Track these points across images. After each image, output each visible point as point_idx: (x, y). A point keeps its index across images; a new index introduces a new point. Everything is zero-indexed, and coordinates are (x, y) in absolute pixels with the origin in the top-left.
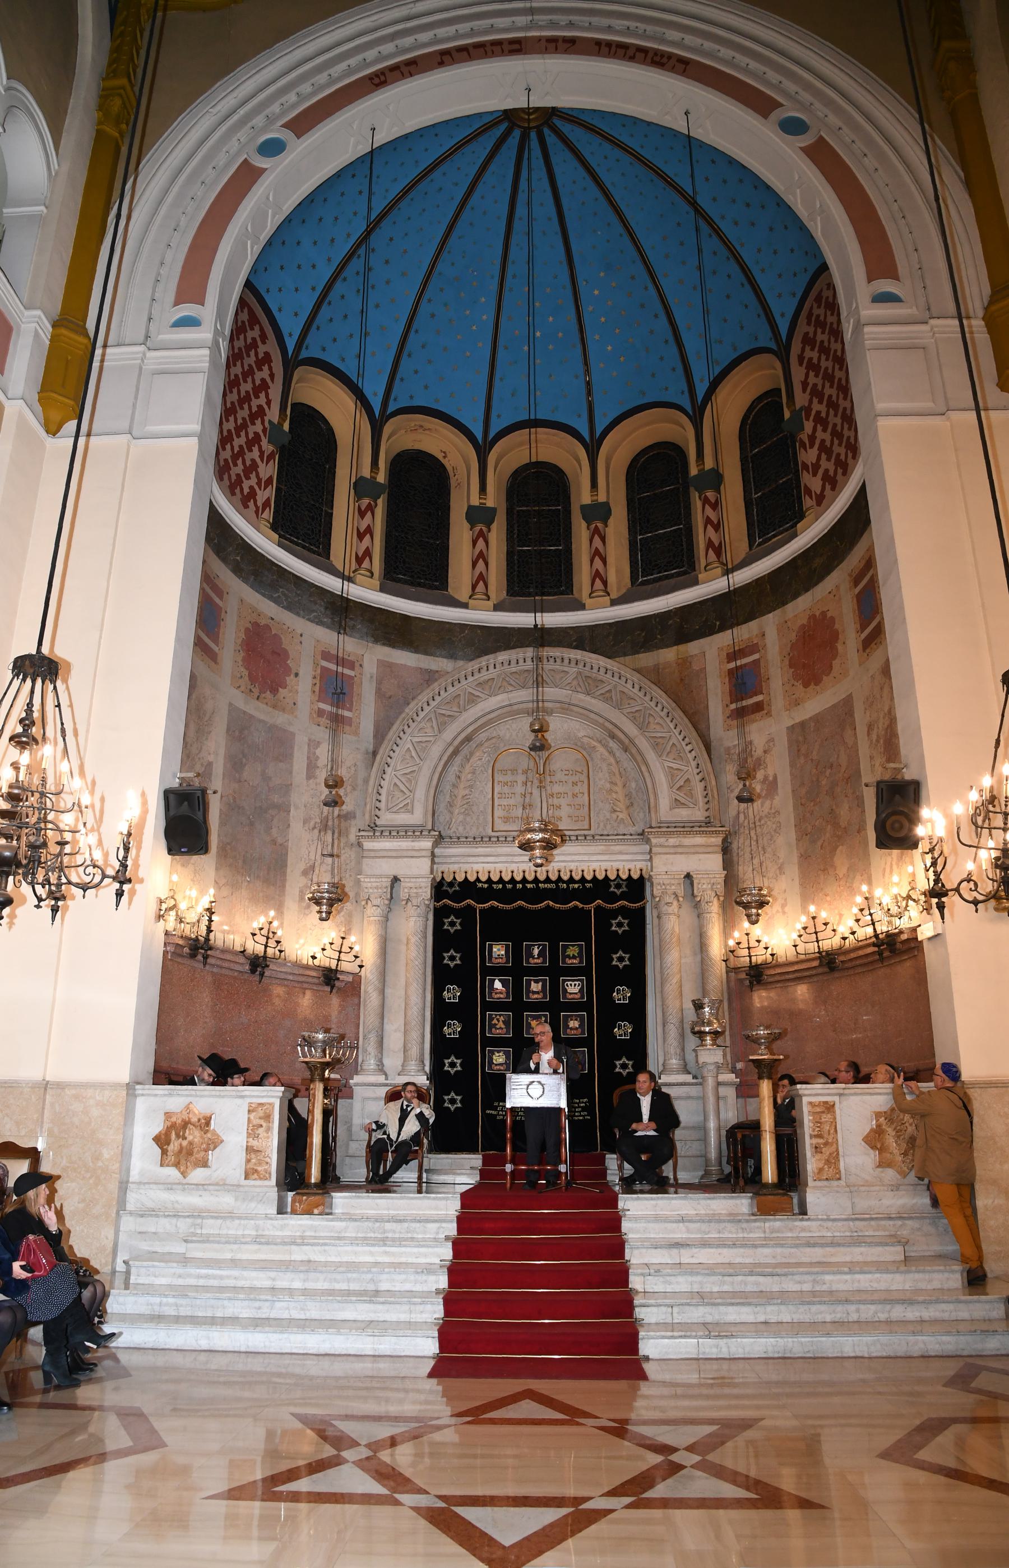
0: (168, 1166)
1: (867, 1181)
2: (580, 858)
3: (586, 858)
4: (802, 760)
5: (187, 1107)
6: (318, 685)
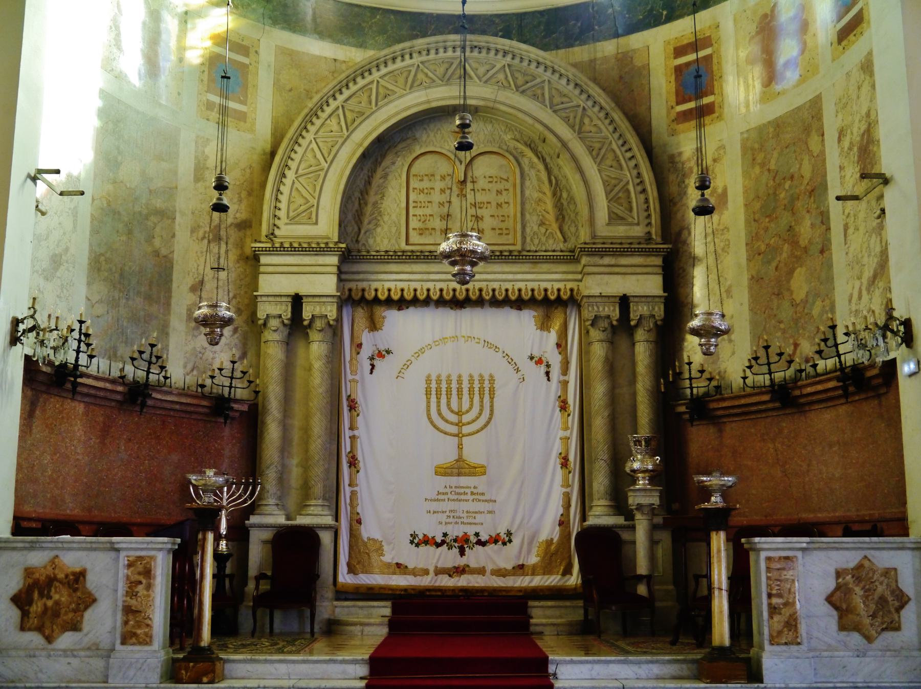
0: (30, 630)
1: (830, 645)
2: (504, 277)
3: (510, 277)
4: (757, 170)
5: (53, 561)
6: (206, 73)
